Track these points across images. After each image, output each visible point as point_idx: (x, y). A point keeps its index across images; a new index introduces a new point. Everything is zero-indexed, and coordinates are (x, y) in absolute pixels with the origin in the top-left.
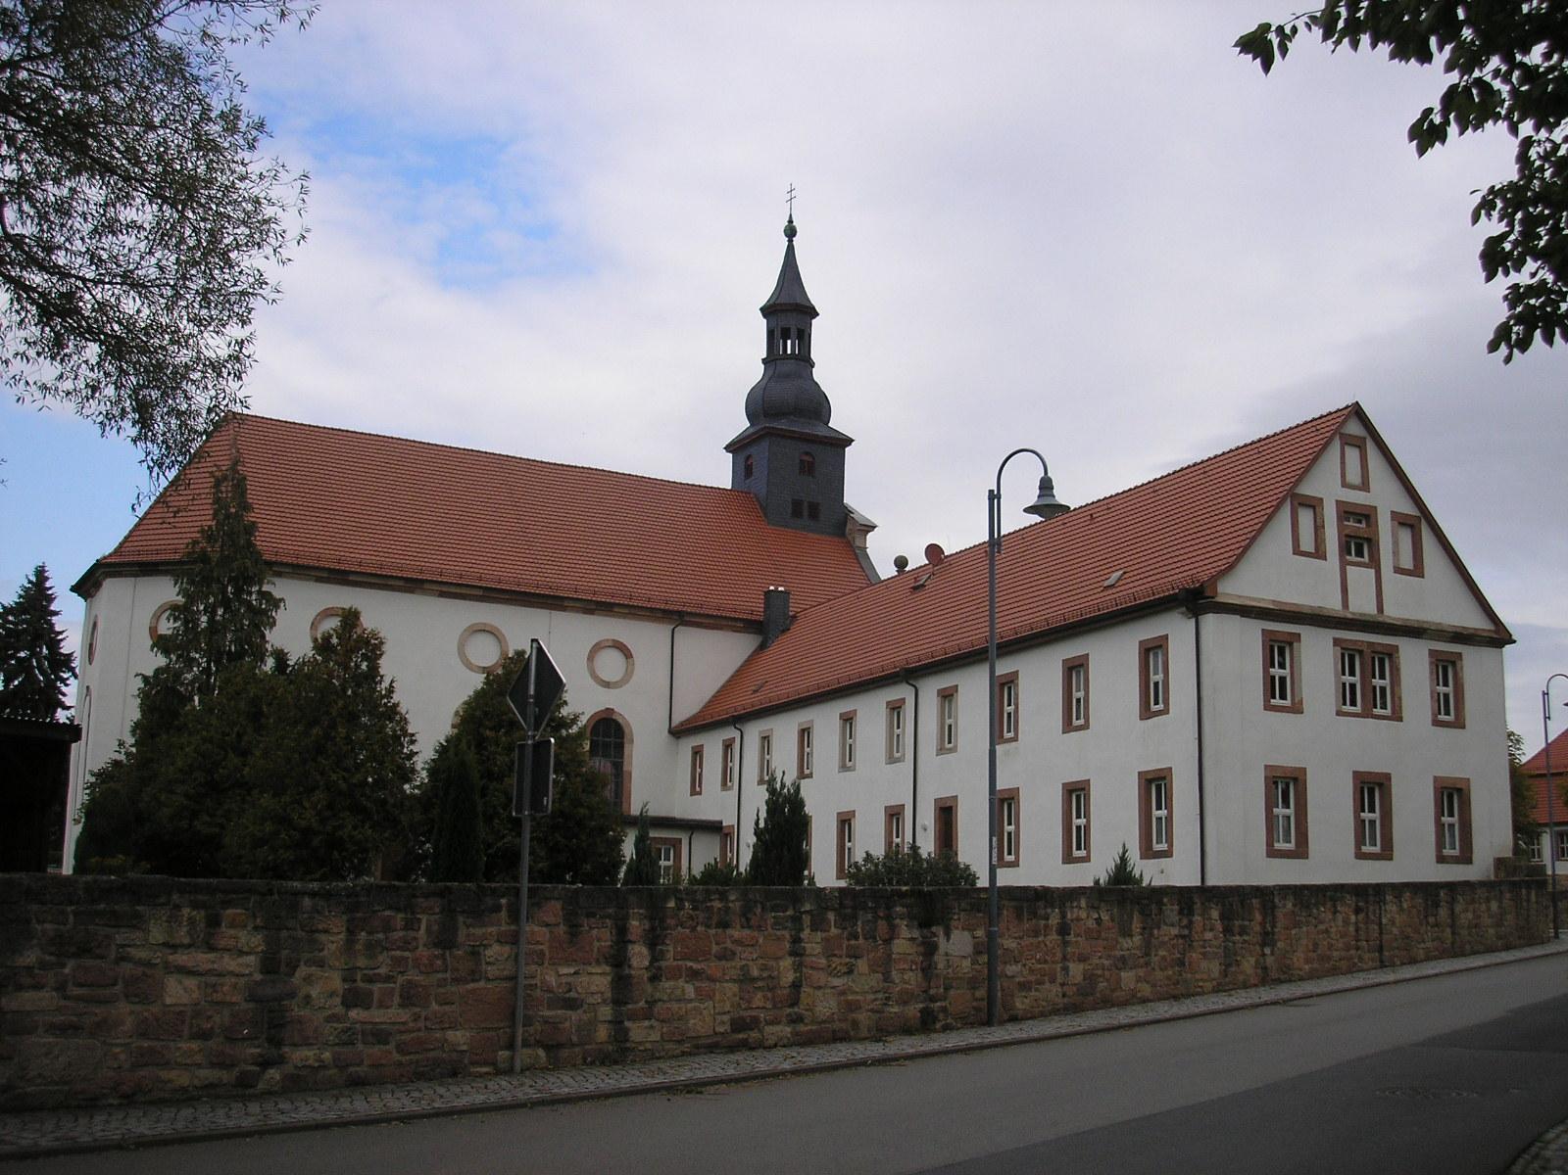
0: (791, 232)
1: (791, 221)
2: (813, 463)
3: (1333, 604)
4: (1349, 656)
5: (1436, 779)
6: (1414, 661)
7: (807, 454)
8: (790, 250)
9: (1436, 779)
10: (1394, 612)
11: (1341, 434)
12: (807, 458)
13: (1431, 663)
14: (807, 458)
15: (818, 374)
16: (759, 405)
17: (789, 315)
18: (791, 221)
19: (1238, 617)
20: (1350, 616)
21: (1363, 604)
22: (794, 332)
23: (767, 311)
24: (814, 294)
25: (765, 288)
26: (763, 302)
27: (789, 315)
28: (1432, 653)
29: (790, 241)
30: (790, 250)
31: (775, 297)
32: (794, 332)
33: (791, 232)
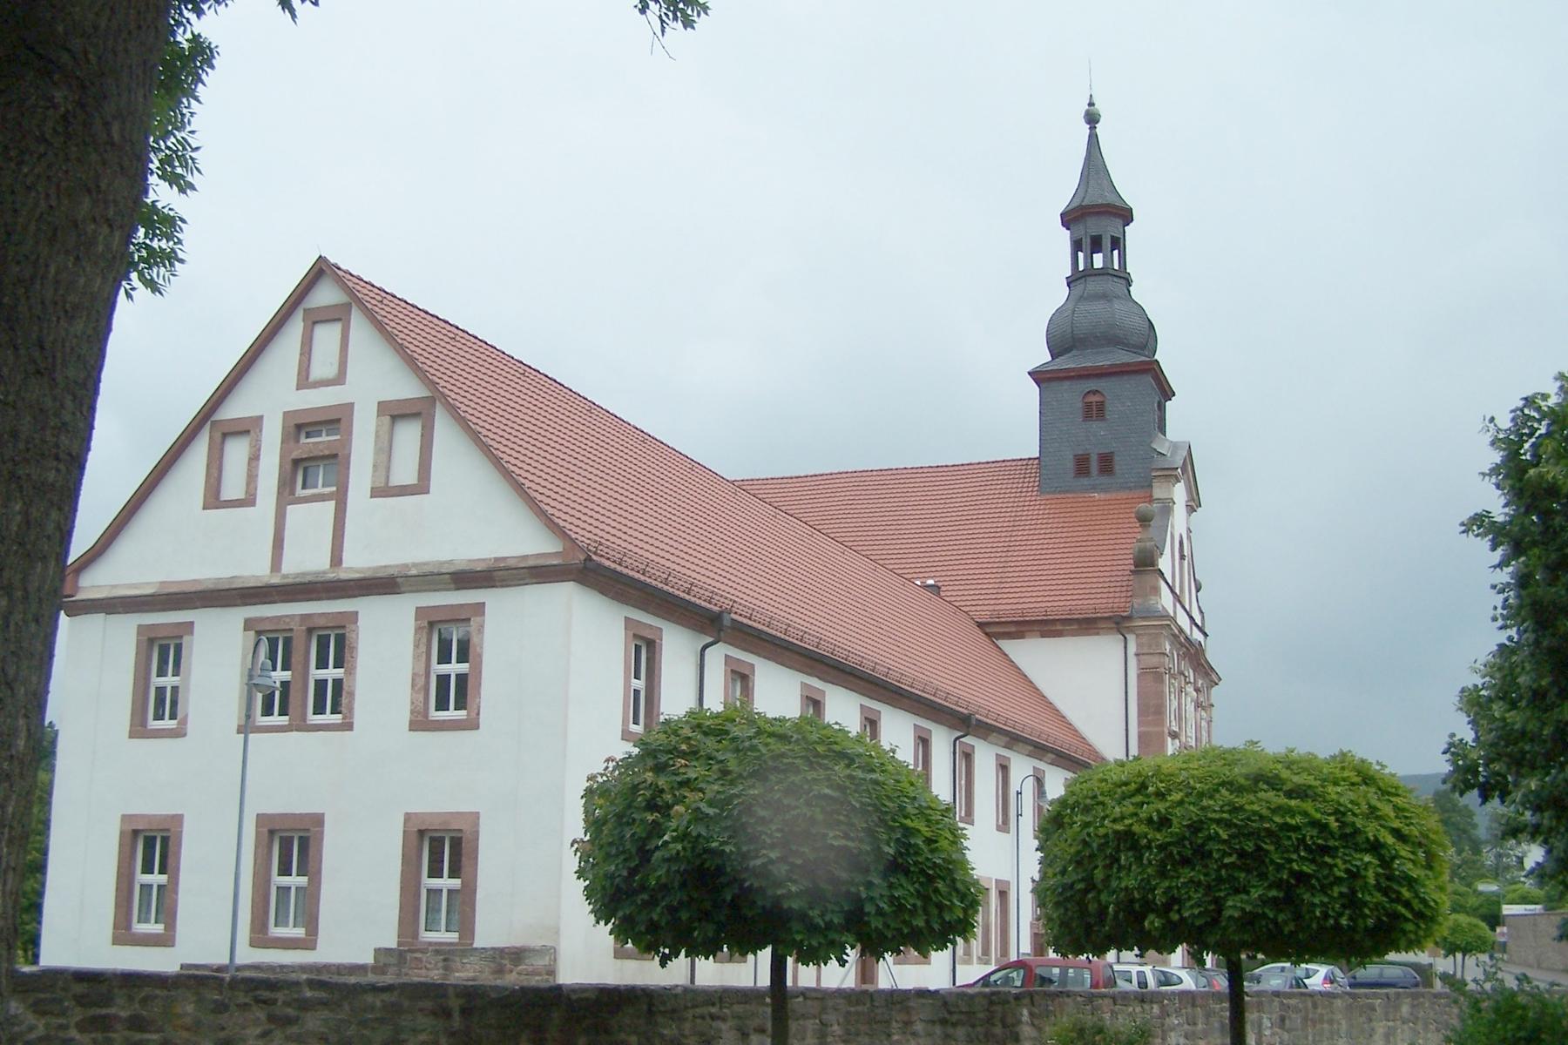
0: (1092, 119)
1: (1091, 104)
2: (1102, 403)
3: (255, 568)
4: (276, 644)
5: (408, 817)
6: (386, 642)
7: (1095, 392)
8: (1093, 140)
9: (408, 817)
10: (359, 560)
11: (346, 308)
12: (1093, 399)
13: (418, 629)
14: (1093, 399)
15: (1138, 292)
16: (1062, 340)
17: (1097, 220)
18: (1091, 104)
19: (102, 615)
20: (343, 576)
21: (307, 556)
22: (1107, 243)
23: (1068, 219)
24: (1128, 190)
25: (1064, 189)
26: (1062, 207)
27: (1097, 220)
28: (248, 624)
29: (1093, 128)
30: (1093, 140)
31: (1081, 194)
32: (1107, 243)
33: (1092, 119)
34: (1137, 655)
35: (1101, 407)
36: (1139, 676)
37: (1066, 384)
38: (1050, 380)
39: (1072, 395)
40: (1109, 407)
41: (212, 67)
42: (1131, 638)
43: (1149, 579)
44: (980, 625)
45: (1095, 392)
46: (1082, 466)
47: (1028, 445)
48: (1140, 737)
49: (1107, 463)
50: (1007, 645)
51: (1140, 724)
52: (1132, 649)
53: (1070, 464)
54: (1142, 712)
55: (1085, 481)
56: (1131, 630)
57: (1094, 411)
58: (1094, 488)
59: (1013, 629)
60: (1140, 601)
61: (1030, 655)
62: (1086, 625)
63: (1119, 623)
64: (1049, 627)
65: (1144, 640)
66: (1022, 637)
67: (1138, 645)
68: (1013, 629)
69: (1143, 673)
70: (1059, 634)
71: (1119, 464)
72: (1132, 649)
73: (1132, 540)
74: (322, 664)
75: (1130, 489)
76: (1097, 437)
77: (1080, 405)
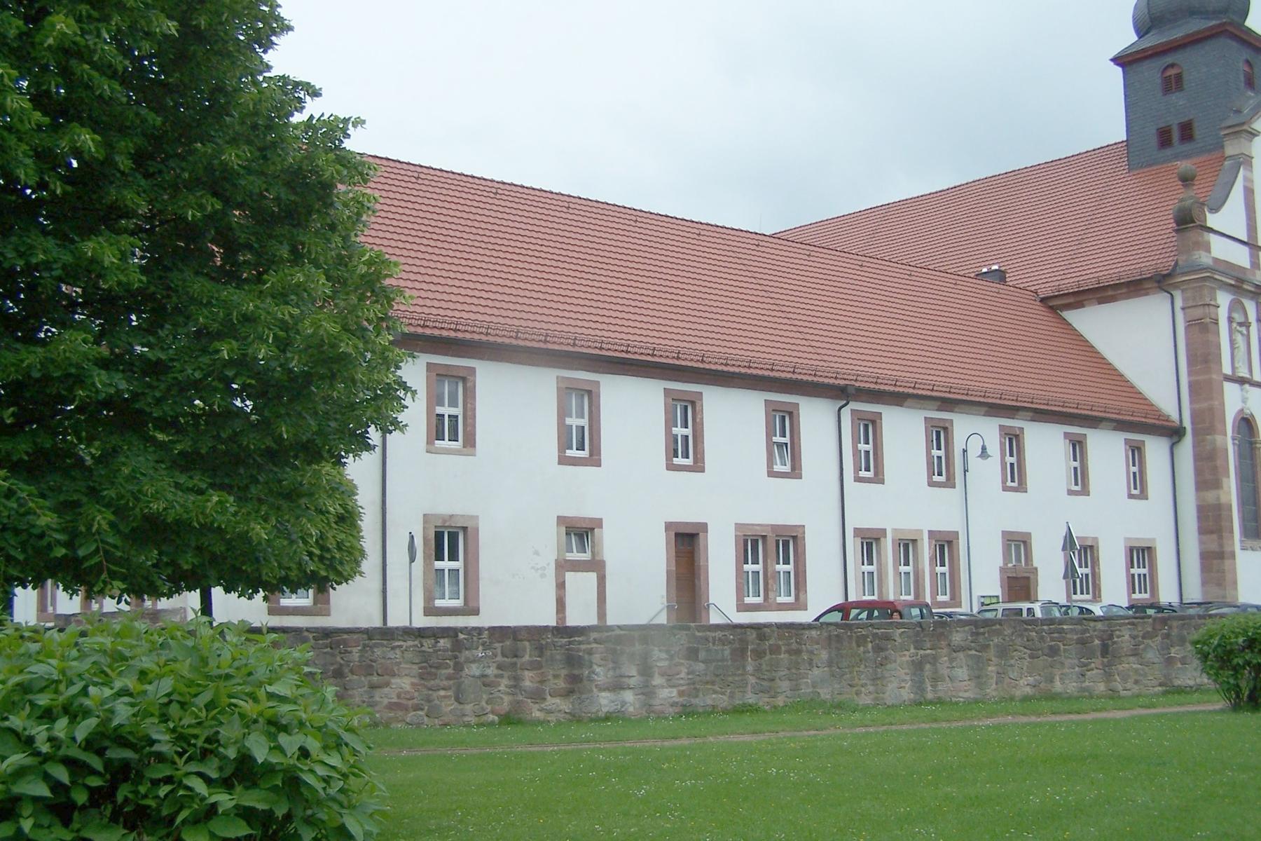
5: (738, 526)
7: (1172, 66)
9: (738, 526)
12: (1172, 72)
14: (1172, 72)
28: (667, 392)
34: (1183, 309)
35: (1179, 78)
36: (1187, 328)
37: (1146, 65)
38: (1131, 63)
39: (1151, 72)
40: (1185, 76)
41: (279, 6)
42: (1178, 296)
43: (1193, 235)
44: (1042, 300)
45: (1172, 66)
46: (1164, 139)
47: (1114, 129)
48: (1190, 386)
49: (1187, 131)
50: (1072, 316)
51: (1190, 373)
52: (1179, 303)
53: (1154, 141)
54: (1191, 362)
55: (1168, 152)
56: (1176, 286)
57: (1173, 83)
58: (1176, 157)
59: (1071, 300)
60: (1184, 257)
61: (1090, 322)
62: (1133, 287)
63: (1161, 282)
64: (1103, 293)
65: (1189, 294)
66: (1083, 306)
67: (1184, 300)
68: (1071, 300)
69: (1191, 324)
70: (1112, 299)
71: (1198, 132)
72: (1179, 303)
73: (1177, 197)
74: (867, 453)
75: (1210, 151)
76: (1177, 108)
77: (1159, 81)
